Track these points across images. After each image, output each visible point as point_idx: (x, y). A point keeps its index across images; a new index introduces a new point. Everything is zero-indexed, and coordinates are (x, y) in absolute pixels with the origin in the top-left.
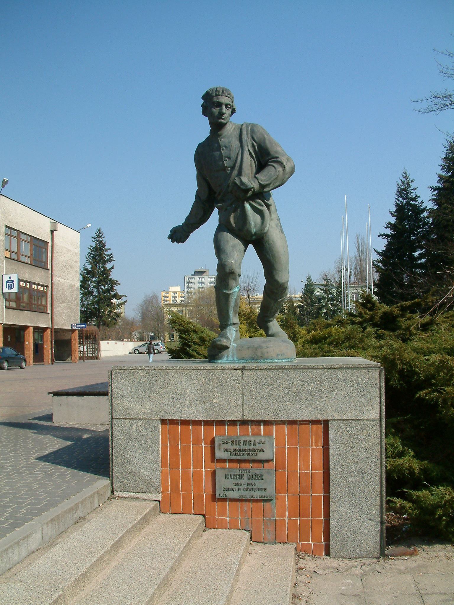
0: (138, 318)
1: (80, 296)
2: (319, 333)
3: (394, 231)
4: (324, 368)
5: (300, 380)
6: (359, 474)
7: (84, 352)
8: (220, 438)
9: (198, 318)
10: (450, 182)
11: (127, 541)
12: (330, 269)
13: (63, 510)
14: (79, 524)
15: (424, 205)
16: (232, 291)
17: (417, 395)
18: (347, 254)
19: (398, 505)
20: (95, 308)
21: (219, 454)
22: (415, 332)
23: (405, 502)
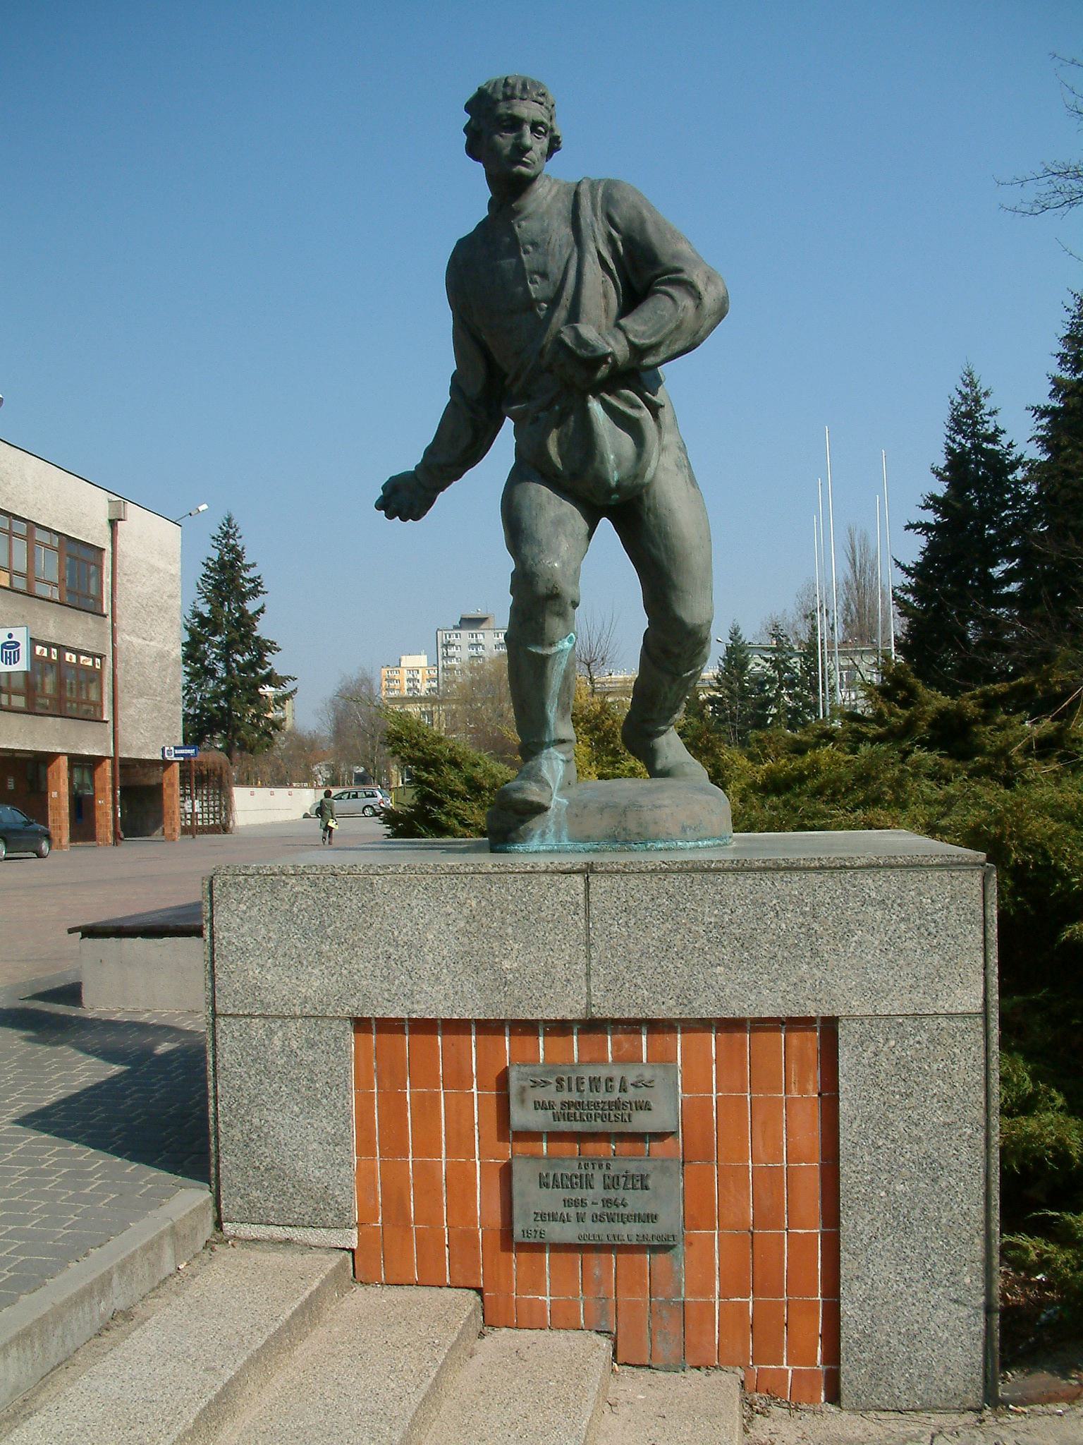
0: (326, 732)
1: (184, 680)
2: (785, 765)
3: (943, 516)
4: (822, 868)
5: (754, 902)
6: (924, 1171)
7: (193, 814)
8: (523, 1069)
9: (470, 731)
10: (1080, 395)
11: (251, 1388)
12: (786, 609)
13: (59, 1300)
14: (113, 1334)
15: (1016, 453)
16: (554, 650)
17: (1066, 934)
18: (830, 574)
19: (1033, 1256)
20: (220, 708)
21: (522, 1117)
22: (1020, 761)
23: (1051, 1247)
